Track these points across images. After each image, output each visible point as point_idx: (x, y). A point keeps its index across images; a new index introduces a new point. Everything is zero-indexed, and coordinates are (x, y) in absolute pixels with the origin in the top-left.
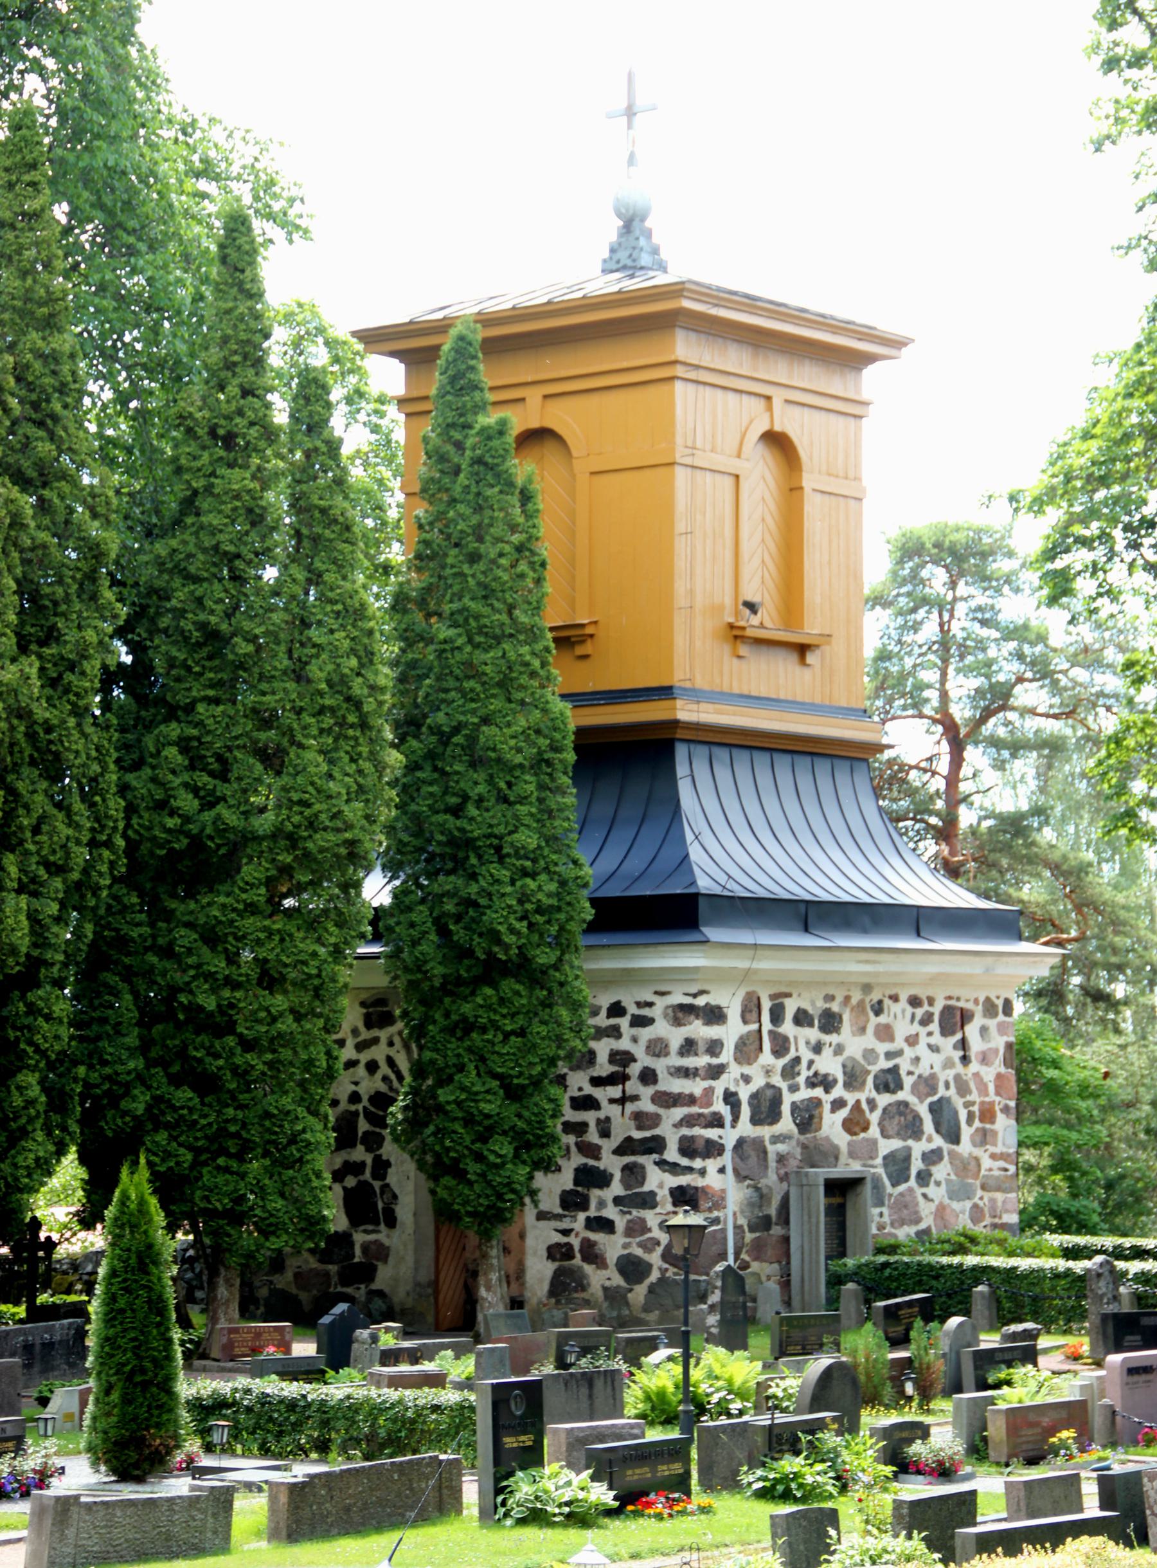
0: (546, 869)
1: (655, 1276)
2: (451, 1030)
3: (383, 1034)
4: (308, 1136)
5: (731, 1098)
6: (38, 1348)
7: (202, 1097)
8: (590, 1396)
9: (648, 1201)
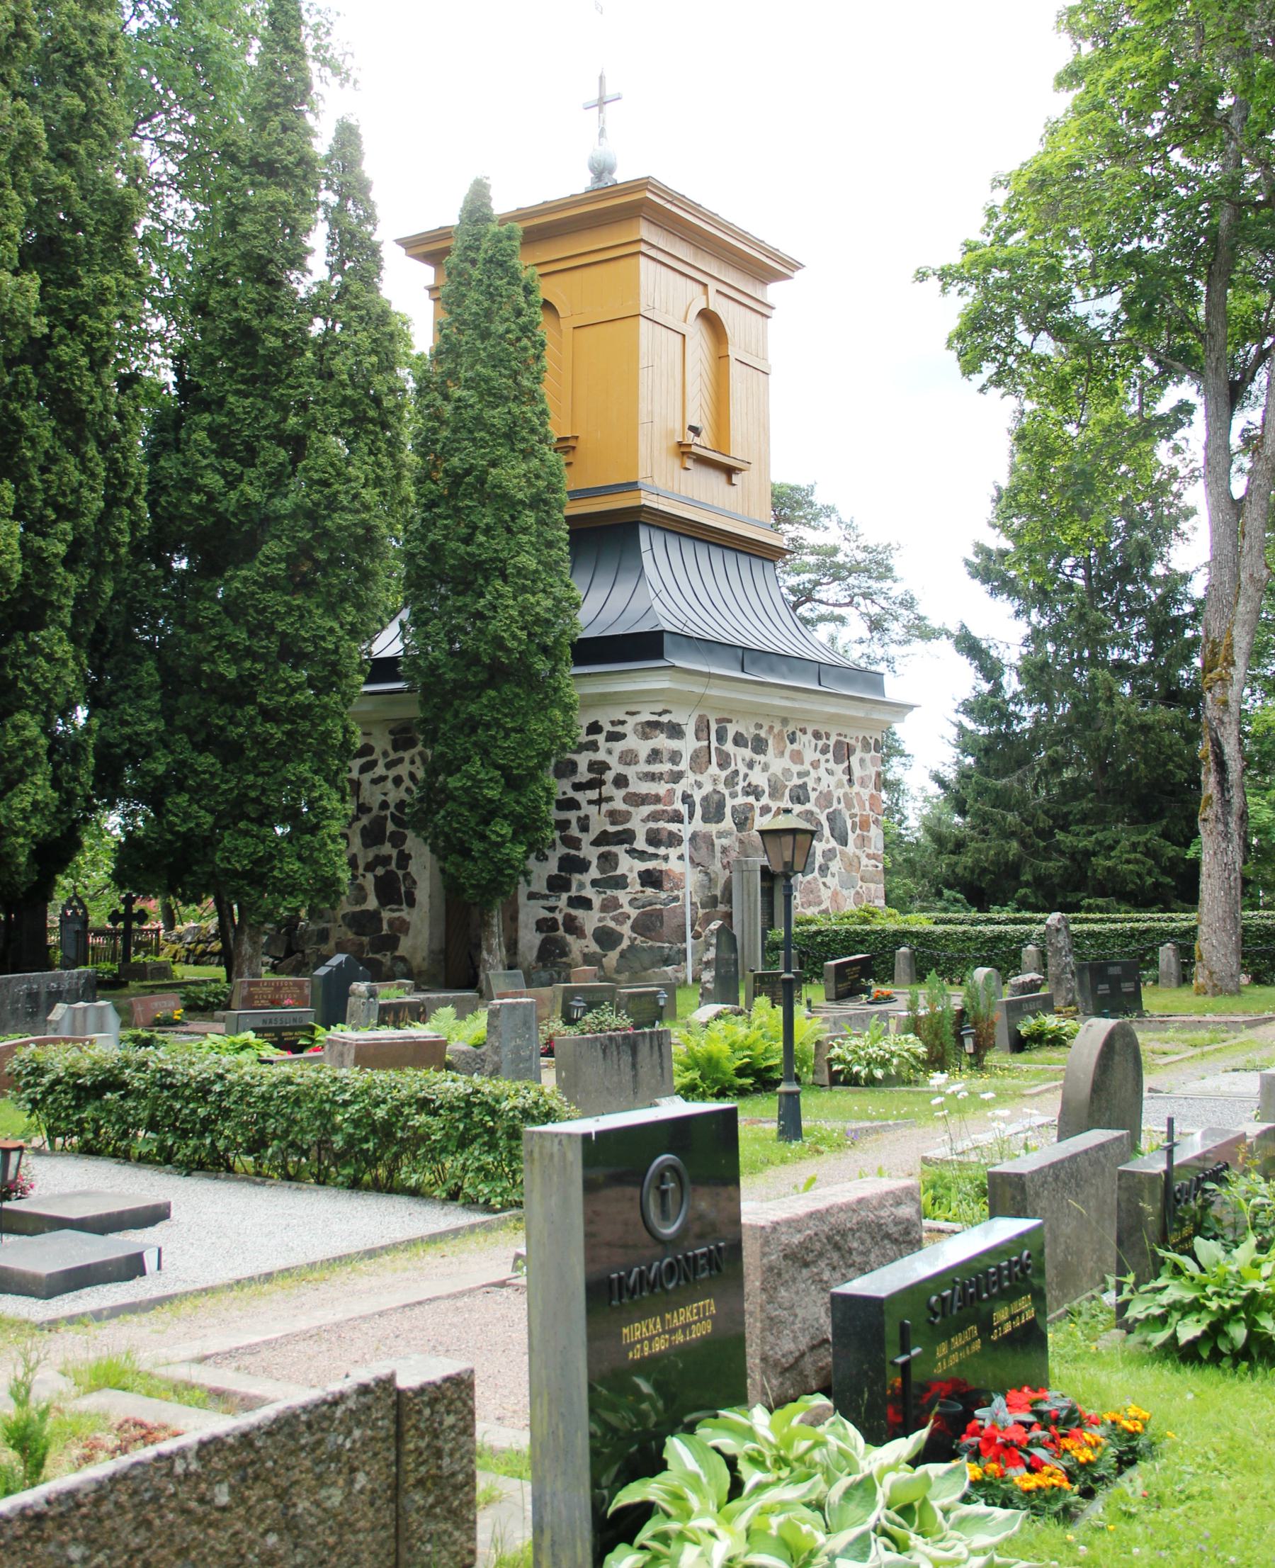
0: (544, 591)
1: (625, 944)
2: (459, 728)
3: (407, 755)
4: (324, 803)
5: (686, 798)
6: (43, 997)
7: (225, 763)
8: (634, 1066)
9: (621, 882)
